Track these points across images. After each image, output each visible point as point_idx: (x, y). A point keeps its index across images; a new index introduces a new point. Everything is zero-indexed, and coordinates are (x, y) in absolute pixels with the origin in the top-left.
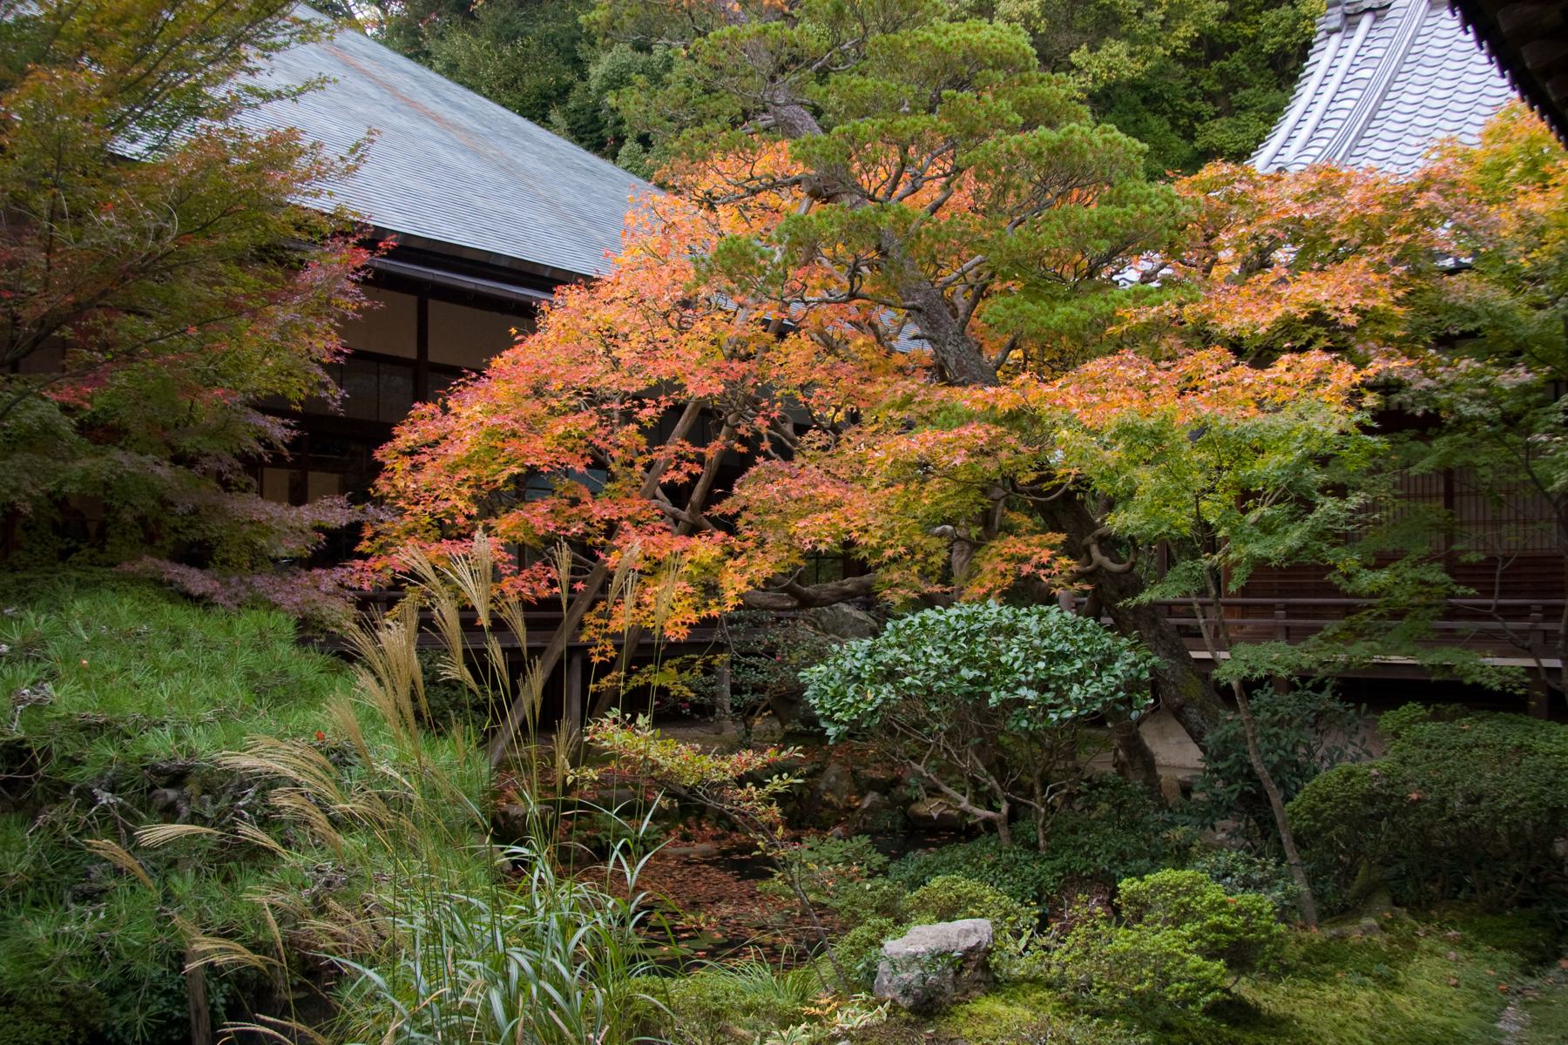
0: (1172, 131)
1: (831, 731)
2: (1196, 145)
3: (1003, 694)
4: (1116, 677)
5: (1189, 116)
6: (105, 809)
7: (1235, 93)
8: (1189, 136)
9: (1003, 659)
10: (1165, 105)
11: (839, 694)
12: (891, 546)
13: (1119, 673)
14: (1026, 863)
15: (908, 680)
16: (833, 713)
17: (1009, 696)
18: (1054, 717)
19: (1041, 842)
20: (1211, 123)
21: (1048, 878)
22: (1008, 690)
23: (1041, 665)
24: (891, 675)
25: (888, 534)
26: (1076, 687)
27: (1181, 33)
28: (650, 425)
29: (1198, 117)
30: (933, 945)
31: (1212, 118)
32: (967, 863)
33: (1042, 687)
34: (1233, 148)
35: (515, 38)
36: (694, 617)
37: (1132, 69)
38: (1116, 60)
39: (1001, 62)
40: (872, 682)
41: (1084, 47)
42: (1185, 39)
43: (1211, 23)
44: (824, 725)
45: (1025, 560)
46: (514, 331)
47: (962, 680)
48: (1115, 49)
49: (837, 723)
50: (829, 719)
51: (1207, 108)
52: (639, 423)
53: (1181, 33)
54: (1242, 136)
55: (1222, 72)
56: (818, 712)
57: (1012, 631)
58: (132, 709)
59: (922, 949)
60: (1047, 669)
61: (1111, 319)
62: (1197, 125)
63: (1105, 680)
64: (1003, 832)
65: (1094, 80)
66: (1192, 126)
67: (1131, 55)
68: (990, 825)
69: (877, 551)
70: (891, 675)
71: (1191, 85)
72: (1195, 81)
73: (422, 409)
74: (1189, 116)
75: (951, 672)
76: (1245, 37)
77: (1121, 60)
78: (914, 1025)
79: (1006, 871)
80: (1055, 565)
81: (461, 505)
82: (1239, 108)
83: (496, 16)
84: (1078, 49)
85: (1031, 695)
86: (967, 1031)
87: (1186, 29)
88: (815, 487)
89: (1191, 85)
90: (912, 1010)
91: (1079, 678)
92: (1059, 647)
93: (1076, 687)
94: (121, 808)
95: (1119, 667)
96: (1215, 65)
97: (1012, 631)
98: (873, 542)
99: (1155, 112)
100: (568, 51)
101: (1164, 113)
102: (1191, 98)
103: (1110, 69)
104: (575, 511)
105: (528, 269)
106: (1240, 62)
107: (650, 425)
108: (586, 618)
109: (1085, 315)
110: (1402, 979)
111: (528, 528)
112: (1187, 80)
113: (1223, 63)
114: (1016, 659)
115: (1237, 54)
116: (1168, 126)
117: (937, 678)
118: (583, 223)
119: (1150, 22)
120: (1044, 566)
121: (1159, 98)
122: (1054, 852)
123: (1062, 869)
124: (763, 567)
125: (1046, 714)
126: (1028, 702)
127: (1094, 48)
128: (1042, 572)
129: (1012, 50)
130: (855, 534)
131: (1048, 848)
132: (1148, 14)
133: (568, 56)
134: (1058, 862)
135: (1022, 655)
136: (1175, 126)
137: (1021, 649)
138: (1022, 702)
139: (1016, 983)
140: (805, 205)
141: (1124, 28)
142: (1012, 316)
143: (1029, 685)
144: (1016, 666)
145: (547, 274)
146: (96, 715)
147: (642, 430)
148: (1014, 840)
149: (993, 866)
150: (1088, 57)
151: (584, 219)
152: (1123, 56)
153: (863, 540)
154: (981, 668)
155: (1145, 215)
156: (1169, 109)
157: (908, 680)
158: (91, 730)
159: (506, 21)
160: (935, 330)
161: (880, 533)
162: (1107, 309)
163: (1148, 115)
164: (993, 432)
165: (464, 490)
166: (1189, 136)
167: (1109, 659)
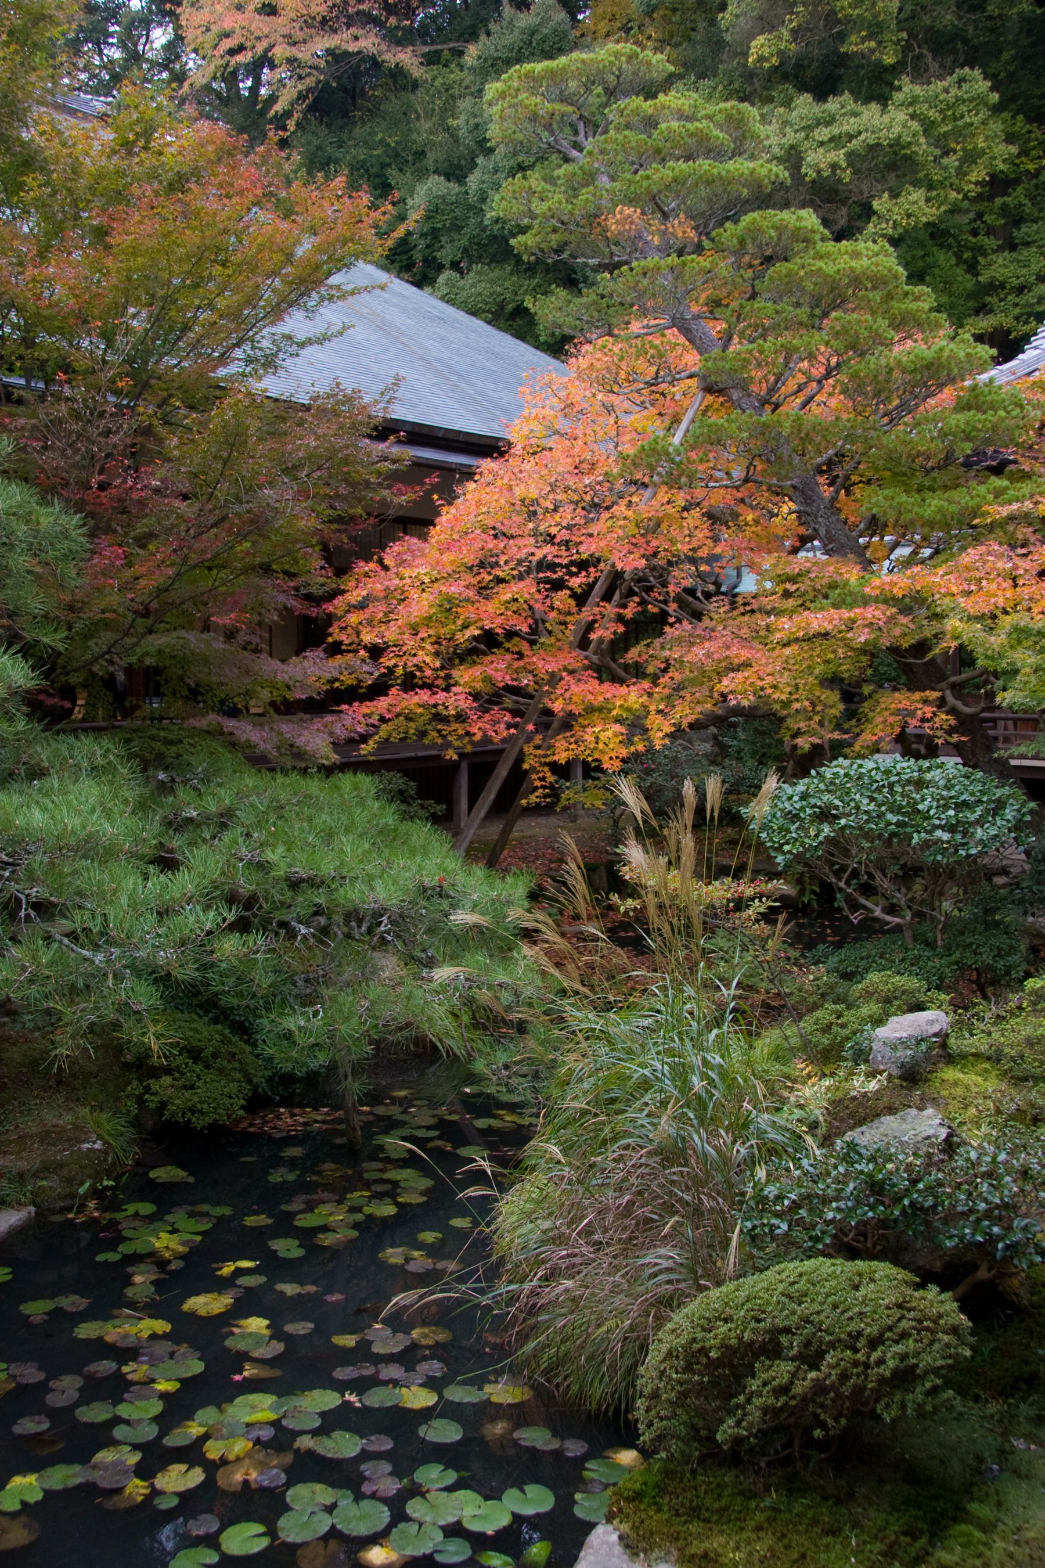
0: (957, 265)
1: (780, 859)
2: (980, 278)
3: (923, 835)
4: (1008, 821)
5: (973, 249)
6: (304, 936)
7: (1019, 229)
8: (972, 268)
9: (920, 807)
10: (951, 240)
11: (784, 830)
12: (797, 700)
13: (1009, 817)
14: (929, 959)
15: (843, 821)
16: (782, 845)
17: (928, 837)
18: (963, 853)
19: (939, 943)
20: (994, 257)
21: (947, 970)
22: (927, 832)
23: (951, 812)
24: (825, 815)
25: (793, 690)
26: (979, 830)
27: (973, 177)
28: (579, 591)
29: (981, 250)
30: (911, 1031)
31: (994, 251)
32: (881, 957)
33: (952, 829)
34: (1015, 282)
35: (328, 164)
36: (624, 752)
37: (929, 213)
38: (915, 207)
39: (878, 281)
40: (812, 822)
41: (886, 195)
42: (977, 183)
43: (1002, 166)
44: (773, 854)
45: (912, 714)
46: (436, 497)
47: (889, 824)
48: (914, 197)
49: (784, 853)
50: (776, 849)
51: (991, 242)
52: (571, 589)
53: (973, 177)
54: (1024, 271)
55: (1004, 208)
56: (769, 844)
57: (920, 784)
58: (328, 868)
59: (905, 1035)
60: (956, 815)
61: (975, 513)
62: (980, 259)
63: (999, 823)
64: (908, 934)
65: (894, 227)
66: (975, 258)
67: (928, 200)
68: (898, 929)
69: (786, 704)
70: (825, 815)
71: (975, 220)
72: (980, 216)
73: (363, 567)
74: (973, 249)
75: (879, 817)
76: (1028, 171)
77: (919, 208)
78: (906, 1088)
79: (912, 965)
80: (937, 719)
81: (428, 659)
82: (1023, 244)
83: (309, 143)
84: (880, 197)
85: (946, 836)
86: (945, 1093)
87: (978, 174)
88: (728, 648)
89: (975, 220)
90: (902, 1077)
91: (980, 822)
92: (962, 798)
93: (979, 830)
94: (314, 935)
95: (1009, 813)
96: (999, 201)
97: (920, 784)
98: (784, 697)
99: (941, 246)
100: (377, 176)
101: (950, 247)
102: (975, 233)
103: (909, 216)
104: (521, 663)
105: (425, 431)
106: (1022, 198)
107: (579, 591)
108: (526, 749)
109: (953, 508)
110: (223, 696)
111: (488, 680)
112: (972, 215)
113: (1007, 199)
114: (931, 807)
115: (1020, 190)
116: (953, 261)
117: (867, 821)
118: (454, 378)
119: (946, 168)
120: (928, 721)
121: (946, 233)
122: (948, 951)
123: (957, 963)
124: (685, 713)
125: (957, 851)
126: (943, 842)
127: (895, 195)
128: (926, 725)
129: (885, 272)
130: (769, 691)
131: (944, 947)
132: (945, 161)
133: (377, 180)
134: (953, 958)
135: (935, 804)
136: (958, 256)
137: (933, 799)
138: (940, 840)
139: (964, 1056)
140: (699, 398)
141: (921, 175)
142: (891, 507)
143: (942, 827)
144: (932, 812)
145: (440, 435)
146: (302, 871)
147: (574, 595)
148: (915, 940)
149: (902, 960)
150: (890, 205)
151: (455, 373)
152: (922, 203)
153: (776, 696)
154: (903, 814)
155: (1002, 419)
156: (954, 244)
157: (843, 821)
158: (295, 884)
159: (319, 148)
160: (808, 505)
161: (788, 689)
162: (972, 503)
163: (935, 249)
164: (888, 613)
165: (428, 647)
166: (972, 268)
167: (1000, 805)
